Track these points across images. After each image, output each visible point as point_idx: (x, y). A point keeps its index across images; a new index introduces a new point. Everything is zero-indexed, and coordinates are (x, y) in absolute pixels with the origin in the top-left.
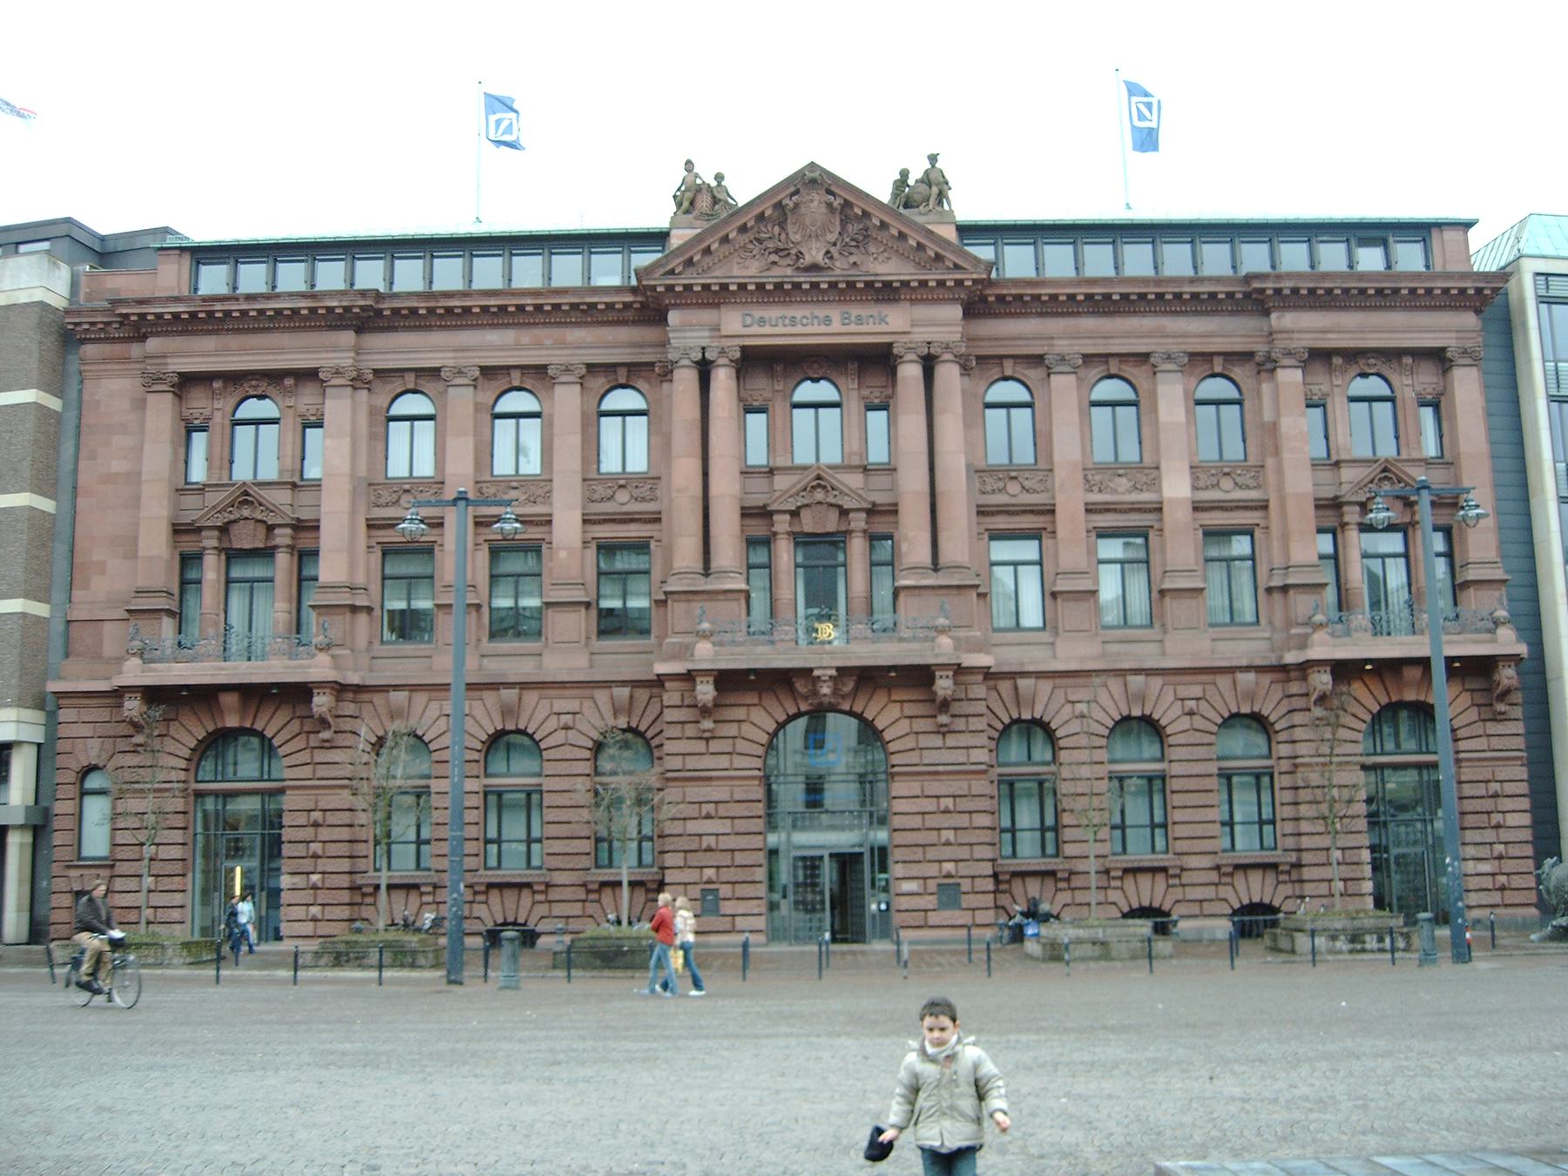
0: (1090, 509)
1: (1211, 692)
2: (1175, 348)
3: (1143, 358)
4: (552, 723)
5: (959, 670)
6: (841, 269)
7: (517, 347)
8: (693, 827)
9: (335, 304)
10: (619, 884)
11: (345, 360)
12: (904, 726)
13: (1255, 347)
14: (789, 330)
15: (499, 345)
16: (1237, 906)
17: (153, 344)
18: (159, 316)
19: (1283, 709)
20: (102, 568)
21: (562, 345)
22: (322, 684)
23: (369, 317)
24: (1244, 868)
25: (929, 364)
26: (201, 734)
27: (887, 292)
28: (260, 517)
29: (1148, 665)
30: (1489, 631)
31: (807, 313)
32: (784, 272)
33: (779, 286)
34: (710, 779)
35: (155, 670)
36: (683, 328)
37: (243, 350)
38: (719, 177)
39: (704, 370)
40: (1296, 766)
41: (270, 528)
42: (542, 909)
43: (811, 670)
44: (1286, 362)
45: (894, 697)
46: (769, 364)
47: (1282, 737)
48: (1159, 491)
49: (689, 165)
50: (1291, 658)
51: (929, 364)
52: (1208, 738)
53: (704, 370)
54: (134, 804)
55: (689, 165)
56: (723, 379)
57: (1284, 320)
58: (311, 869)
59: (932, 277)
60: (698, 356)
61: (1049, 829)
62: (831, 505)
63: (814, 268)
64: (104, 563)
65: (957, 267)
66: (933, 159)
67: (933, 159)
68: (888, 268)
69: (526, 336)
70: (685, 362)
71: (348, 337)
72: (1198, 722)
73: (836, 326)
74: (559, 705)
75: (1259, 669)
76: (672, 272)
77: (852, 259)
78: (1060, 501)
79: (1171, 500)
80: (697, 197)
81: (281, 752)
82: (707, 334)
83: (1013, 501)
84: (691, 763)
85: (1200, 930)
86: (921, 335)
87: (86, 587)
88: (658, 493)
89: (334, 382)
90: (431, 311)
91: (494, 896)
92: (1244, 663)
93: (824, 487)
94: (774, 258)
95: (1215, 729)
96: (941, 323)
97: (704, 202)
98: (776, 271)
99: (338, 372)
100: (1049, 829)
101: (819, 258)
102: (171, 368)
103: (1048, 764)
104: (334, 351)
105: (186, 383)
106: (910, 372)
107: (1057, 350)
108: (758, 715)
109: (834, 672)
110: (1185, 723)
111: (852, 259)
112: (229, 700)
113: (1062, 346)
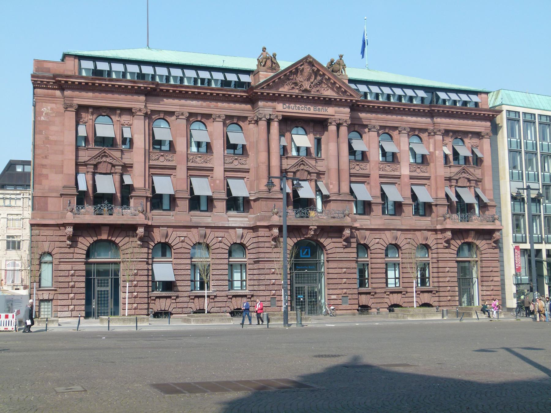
0: (381, 176)
1: (226, 235)
2: (406, 126)
3: (395, 128)
4: (177, 240)
5: (352, 228)
6: (314, 93)
7: (202, 107)
8: (267, 277)
9: (142, 85)
10: (204, 297)
11: (142, 106)
12: (332, 245)
13: (429, 128)
14: (297, 111)
15: (195, 106)
16: (390, 305)
17: (68, 93)
18: (73, 82)
19: (435, 242)
20: (46, 177)
21: (217, 107)
22: (141, 225)
23: (154, 92)
24: (392, 293)
25: (338, 126)
26: (92, 242)
27: (328, 102)
28: (110, 161)
29: (398, 227)
30: (493, 221)
31: (303, 106)
32: (296, 91)
33: (297, 96)
34: (273, 261)
35: (79, 217)
36: (264, 107)
37: (103, 98)
38: (274, 55)
39: (269, 122)
40: (438, 261)
41: (113, 166)
42: (174, 305)
43: (309, 226)
44: (438, 133)
45: (330, 236)
46: (288, 123)
47: (434, 251)
48: (400, 171)
49: (264, 49)
50: (439, 227)
51: (338, 126)
52: (187, 251)
53: (269, 122)
54: (63, 267)
55: (264, 49)
56: (275, 126)
57: (438, 120)
58: (133, 291)
59: (344, 98)
60: (268, 117)
61: (397, 278)
62: (306, 171)
63: (306, 91)
64: (47, 175)
65: (351, 95)
66: (341, 57)
67: (341, 57)
68: (329, 93)
69: (205, 104)
70: (263, 119)
71: (143, 98)
72: (184, 244)
73: (312, 111)
74: (217, 234)
75: (244, 228)
76: (263, 88)
77: (317, 89)
78: (372, 173)
79: (404, 175)
80: (267, 61)
81: (123, 248)
82: (271, 110)
83: (357, 172)
84: (267, 255)
85: (226, 322)
86: (338, 116)
87: (41, 184)
88: (247, 162)
89: (138, 113)
90: (174, 91)
91: (196, 299)
92: (424, 228)
93: (304, 164)
94: (293, 86)
95: (190, 248)
96: (343, 113)
97: (269, 63)
98: (293, 91)
99: (140, 110)
100: (397, 278)
101: (308, 88)
102: (75, 102)
103: (397, 258)
104: (137, 102)
105: (81, 109)
106: (332, 128)
107: (372, 124)
108: (459, 242)
109: (316, 227)
110: (407, 246)
111: (317, 89)
112: (473, 234)
113: (373, 122)
